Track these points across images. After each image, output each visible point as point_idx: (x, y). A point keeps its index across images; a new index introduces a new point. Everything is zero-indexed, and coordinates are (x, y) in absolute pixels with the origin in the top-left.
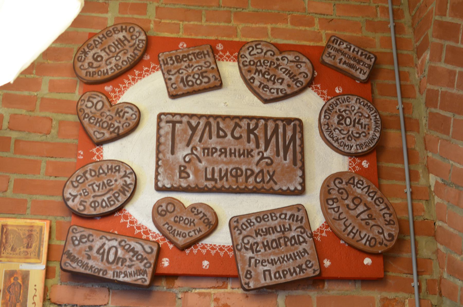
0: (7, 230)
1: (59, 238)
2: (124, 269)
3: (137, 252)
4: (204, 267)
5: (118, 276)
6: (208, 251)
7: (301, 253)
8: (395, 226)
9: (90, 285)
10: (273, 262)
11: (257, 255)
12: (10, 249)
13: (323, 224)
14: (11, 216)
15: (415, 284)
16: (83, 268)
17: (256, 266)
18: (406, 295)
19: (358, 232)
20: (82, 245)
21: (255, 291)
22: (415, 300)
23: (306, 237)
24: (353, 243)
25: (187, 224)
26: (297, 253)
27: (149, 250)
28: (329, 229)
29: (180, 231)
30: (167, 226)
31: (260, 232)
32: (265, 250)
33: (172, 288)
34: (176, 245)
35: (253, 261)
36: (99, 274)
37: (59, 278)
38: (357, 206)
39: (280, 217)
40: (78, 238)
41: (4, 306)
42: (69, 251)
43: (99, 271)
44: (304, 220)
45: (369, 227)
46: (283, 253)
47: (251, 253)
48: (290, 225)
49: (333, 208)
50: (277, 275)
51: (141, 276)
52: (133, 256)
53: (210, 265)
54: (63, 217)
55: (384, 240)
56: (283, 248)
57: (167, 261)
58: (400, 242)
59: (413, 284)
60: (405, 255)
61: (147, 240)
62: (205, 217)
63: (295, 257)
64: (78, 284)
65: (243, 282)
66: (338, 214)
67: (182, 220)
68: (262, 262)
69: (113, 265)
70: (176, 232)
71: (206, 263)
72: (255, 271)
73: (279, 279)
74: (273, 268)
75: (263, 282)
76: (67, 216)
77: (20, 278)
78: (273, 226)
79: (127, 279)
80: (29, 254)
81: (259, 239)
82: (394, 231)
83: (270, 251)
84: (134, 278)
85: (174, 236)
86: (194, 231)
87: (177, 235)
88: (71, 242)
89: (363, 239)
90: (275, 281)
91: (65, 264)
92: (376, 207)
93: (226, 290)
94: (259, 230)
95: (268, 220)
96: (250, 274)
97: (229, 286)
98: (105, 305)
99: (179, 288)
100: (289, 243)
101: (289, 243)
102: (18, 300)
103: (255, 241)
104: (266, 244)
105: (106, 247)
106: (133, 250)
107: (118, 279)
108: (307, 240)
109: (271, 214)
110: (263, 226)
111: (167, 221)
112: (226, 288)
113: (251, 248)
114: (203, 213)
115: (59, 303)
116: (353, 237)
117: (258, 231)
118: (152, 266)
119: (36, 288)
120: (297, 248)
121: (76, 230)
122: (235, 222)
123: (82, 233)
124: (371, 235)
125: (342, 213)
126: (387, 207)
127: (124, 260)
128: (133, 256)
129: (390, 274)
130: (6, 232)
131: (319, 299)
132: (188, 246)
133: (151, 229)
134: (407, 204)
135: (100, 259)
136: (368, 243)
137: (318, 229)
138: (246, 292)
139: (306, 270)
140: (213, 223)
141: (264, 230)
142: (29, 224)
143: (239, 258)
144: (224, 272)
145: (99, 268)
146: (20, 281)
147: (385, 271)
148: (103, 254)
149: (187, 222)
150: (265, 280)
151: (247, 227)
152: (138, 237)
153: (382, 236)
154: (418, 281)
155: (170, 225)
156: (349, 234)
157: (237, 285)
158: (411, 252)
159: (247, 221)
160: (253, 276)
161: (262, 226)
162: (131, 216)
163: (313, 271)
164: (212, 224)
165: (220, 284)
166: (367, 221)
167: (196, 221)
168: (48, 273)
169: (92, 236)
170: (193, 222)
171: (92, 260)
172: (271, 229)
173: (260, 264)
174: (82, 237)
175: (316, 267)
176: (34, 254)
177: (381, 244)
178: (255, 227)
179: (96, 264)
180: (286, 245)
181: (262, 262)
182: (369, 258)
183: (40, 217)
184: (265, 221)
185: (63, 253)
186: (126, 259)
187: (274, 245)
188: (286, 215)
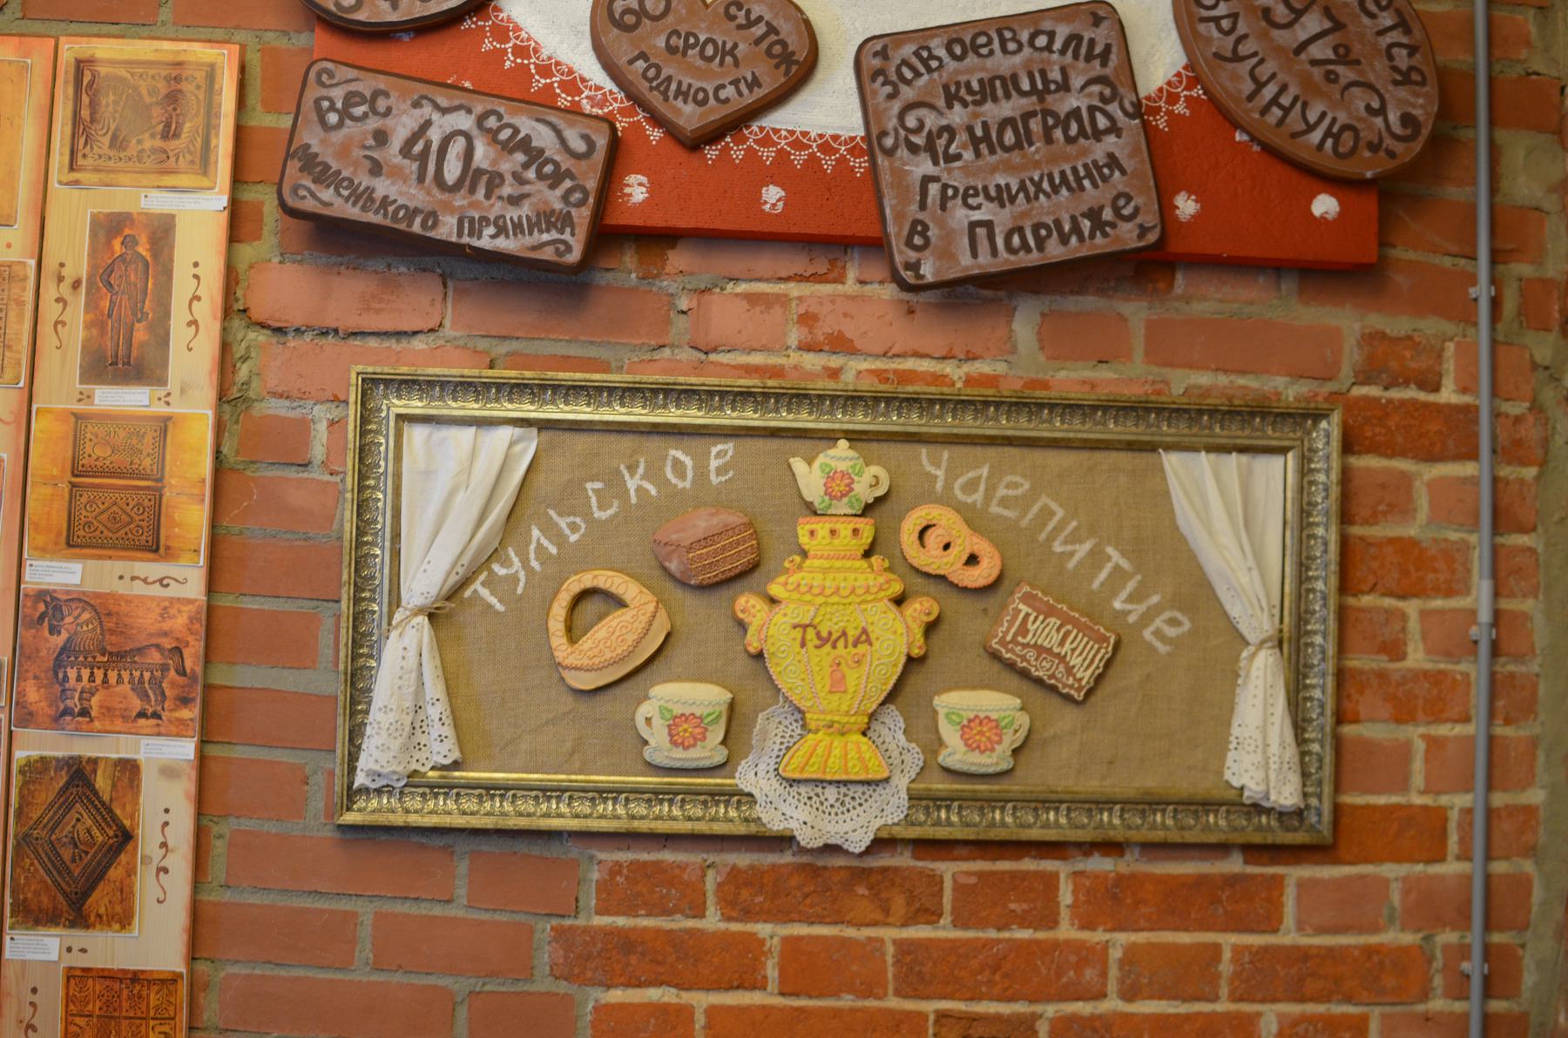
0: (94, 76)
1: (271, 107)
2: (496, 209)
3: (541, 151)
4: (767, 207)
5: (475, 232)
6: (780, 152)
7: (1099, 169)
8: (1426, 89)
9: (380, 264)
10: (1002, 197)
11: (949, 171)
12: (106, 140)
13: (1178, 74)
14: (105, 29)
15: (1482, 291)
16: (354, 204)
17: (943, 207)
18: (1448, 327)
19: (1299, 105)
20: (350, 128)
21: (938, 292)
22: (1476, 344)
23: (1119, 114)
24: (1277, 140)
25: (710, 59)
26: (1085, 166)
27: (579, 146)
28: (1198, 92)
29: (686, 81)
30: (641, 64)
31: (963, 92)
32: (978, 154)
33: (657, 276)
34: (672, 131)
35: (934, 189)
36: (410, 225)
37: (274, 240)
38: (1299, 14)
39: (1031, 43)
40: (339, 105)
41: (94, 331)
42: (308, 146)
43: (412, 213)
44: (1114, 58)
45: (1335, 89)
46: (1037, 165)
47: (930, 163)
48: (1063, 70)
49: (1216, 20)
50: (1016, 240)
51: (554, 235)
52: (526, 166)
53: (787, 201)
55: (1385, 134)
56: (1037, 151)
57: (641, 184)
58: (1440, 145)
59: (1473, 292)
60: (1453, 192)
61: (575, 111)
62: (773, 38)
63: (1079, 180)
65: (898, 259)
66: (1232, 38)
67: (693, 46)
68: (965, 196)
69: (458, 196)
70: (673, 86)
71: (772, 195)
72: (942, 224)
73: (1022, 253)
74: (1003, 218)
75: (966, 263)
76: (298, 32)
77: (143, 239)
78: (1007, 74)
79: (505, 244)
80: (173, 159)
81: (957, 116)
82: (1422, 106)
83: (993, 159)
84: (528, 241)
85: (666, 99)
86: (735, 83)
87: (676, 98)
88: (315, 118)
89: (1316, 127)
90: (1006, 260)
91: (295, 190)
92: (1366, 20)
93: (840, 287)
94: (958, 84)
95: (991, 53)
96: (923, 234)
97: (852, 274)
98: (431, 330)
99: (680, 278)
100: (1058, 134)
101: (1058, 134)
102: (138, 314)
103: (944, 122)
104: (979, 132)
105: (435, 135)
106: (525, 145)
107: (475, 243)
108: (1120, 125)
109: (1000, 33)
110: (973, 71)
111: (644, 48)
112: (840, 280)
113: (930, 147)
114: (768, 24)
116: (1281, 122)
117: (953, 89)
118: (591, 200)
119: (197, 271)
120: (1084, 152)
121: (331, 75)
122: (876, 54)
123: (353, 87)
124: (1343, 118)
125: (1245, 36)
126: (1403, 24)
127: (495, 180)
128: (526, 166)
129: (1400, 253)
130: (91, 83)
131: (1151, 326)
132: (713, 135)
133: (586, 76)
134: (1471, 20)
135: (414, 176)
136: (1329, 142)
137: (1160, 90)
138: (906, 296)
139: (1113, 225)
140: (801, 56)
141: (975, 86)
142: (170, 58)
143: (886, 178)
144: (836, 226)
145: (412, 205)
146: (143, 250)
147: (1384, 243)
148: (423, 157)
149: (710, 51)
150: (975, 254)
151: (918, 74)
152: (542, 103)
153: (1379, 121)
154: (1493, 281)
155: (652, 60)
156: (1265, 111)
157: (877, 270)
158: (1474, 182)
159: (917, 54)
160: (933, 240)
161: (970, 71)
162: (517, 29)
163: (1137, 232)
164: (797, 62)
165: (821, 267)
166: (1331, 67)
167: (742, 48)
168: (238, 223)
169: (387, 95)
170: (732, 53)
171: (387, 177)
172: (998, 83)
173: (959, 201)
174: (352, 99)
175: (1150, 218)
176: (188, 157)
177: (1374, 147)
178: (945, 75)
179: (399, 191)
180: (1049, 140)
181: (965, 196)
182: (1332, 195)
183: (206, 33)
184: (980, 55)
185: (288, 156)
186: (501, 176)
187: (1009, 137)
188: (1051, 35)
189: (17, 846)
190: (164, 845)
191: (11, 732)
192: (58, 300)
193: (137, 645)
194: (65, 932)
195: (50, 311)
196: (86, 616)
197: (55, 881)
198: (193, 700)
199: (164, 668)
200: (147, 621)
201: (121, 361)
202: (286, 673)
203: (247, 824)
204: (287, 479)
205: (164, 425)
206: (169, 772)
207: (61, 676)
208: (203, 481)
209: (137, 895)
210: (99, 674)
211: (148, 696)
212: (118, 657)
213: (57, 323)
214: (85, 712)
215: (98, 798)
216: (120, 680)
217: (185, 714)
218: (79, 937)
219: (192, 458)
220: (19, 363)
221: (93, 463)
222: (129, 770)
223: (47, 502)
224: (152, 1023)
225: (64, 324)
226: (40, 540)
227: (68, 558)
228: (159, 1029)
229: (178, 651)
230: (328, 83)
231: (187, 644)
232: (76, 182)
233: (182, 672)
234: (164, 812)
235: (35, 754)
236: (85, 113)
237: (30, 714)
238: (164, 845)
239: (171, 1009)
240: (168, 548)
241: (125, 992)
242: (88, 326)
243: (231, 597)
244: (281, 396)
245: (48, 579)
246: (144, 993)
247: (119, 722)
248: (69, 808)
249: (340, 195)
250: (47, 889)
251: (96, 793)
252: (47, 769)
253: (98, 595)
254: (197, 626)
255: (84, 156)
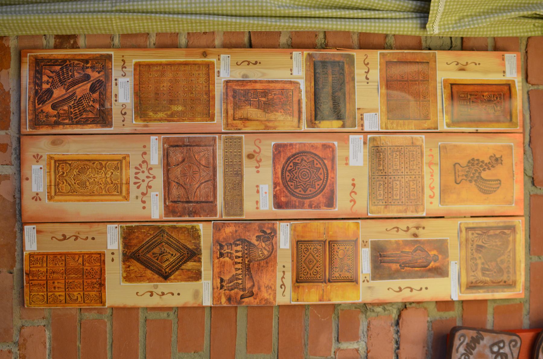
0: (508, 234)
12: (480, 243)
37: (438, 317)
40: (501, 351)
42: (483, 339)
54: (529, 313)
64: (430, 347)
76: (530, 319)
80: (473, 274)
91: (463, 336)
115: (400, 322)
119: (424, 289)
121: (514, 346)
146: (432, 264)
168: (445, 305)
189: (159, 228)
190: (163, 294)
191: (211, 221)
192: (408, 228)
193: (253, 276)
194: (121, 252)
195: (402, 225)
196: (266, 253)
197: (144, 245)
198: (230, 303)
199: (244, 289)
200: (264, 279)
201: (380, 255)
202: (244, 341)
203: (175, 327)
204: (331, 333)
205: (354, 281)
206: (197, 294)
207: (238, 242)
208: (329, 300)
209: (139, 284)
210: (239, 260)
211: (230, 283)
212: (248, 269)
213: (398, 228)
214: (222, 255)
215: (183, 263)
216: (237, 269)
217: (224, 300)
218: (119, 258)
219: (342, 296)
220: (379, 212)
221: (335, 250)
222: (197, 276)
223: (316, 231)
224: (82, 293)
225: (398, 231)
226: (299, 229)
227: (291, 242)
228: (79, 296)
229: (252, 294)
230: (511, 345)
231: (255, 299)
232: (461, 231)
233: (242, 297)
234: (178, 293)
235: (201, 233)
236: (491, 232)
237: (220, 230)
238: (163, 294)
239: (89, 301)
240: (298, 287)
241: (94, 281)
242: (397, 242)
243: (277, 313)
244: (368, 327)
245: (281, 233)
246: (95, 289)
247: (218, 270)
248: (177, 250)
249: (462, 355)
250: (140, 242)
251: (185, 262)
252: (195, 239)
253: (275, 257)
254: (264, 302)
255: (473, 234)
